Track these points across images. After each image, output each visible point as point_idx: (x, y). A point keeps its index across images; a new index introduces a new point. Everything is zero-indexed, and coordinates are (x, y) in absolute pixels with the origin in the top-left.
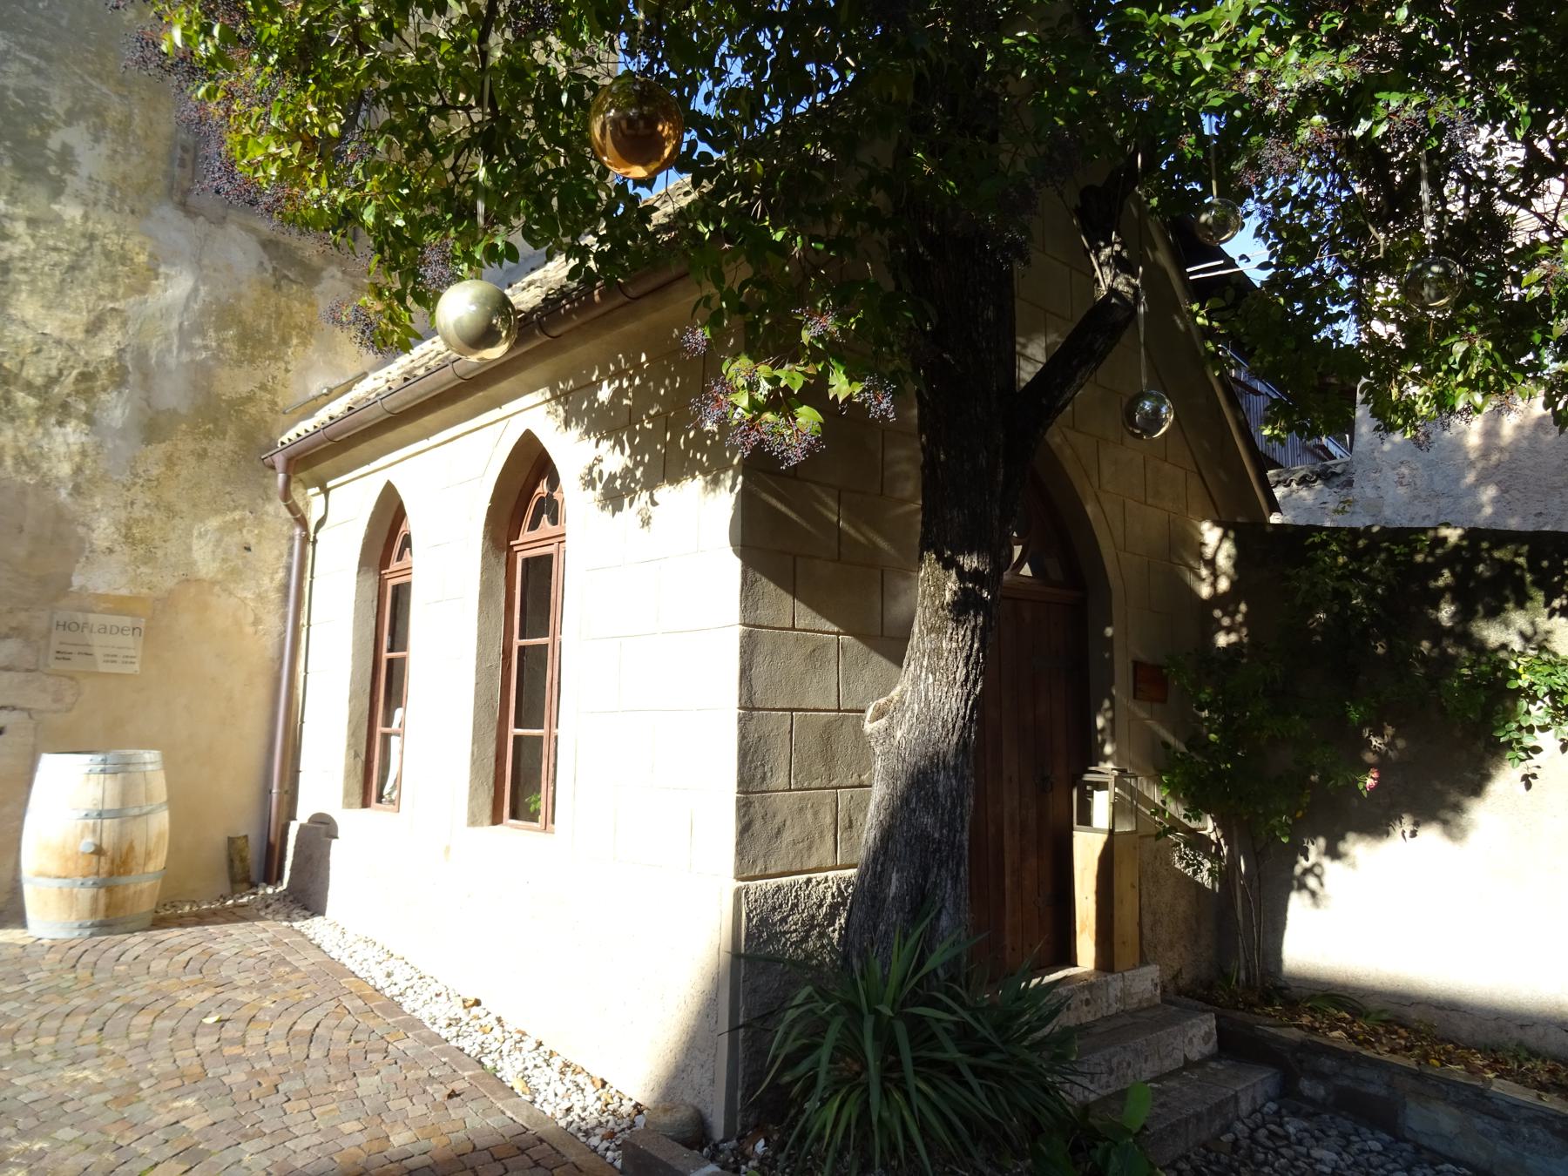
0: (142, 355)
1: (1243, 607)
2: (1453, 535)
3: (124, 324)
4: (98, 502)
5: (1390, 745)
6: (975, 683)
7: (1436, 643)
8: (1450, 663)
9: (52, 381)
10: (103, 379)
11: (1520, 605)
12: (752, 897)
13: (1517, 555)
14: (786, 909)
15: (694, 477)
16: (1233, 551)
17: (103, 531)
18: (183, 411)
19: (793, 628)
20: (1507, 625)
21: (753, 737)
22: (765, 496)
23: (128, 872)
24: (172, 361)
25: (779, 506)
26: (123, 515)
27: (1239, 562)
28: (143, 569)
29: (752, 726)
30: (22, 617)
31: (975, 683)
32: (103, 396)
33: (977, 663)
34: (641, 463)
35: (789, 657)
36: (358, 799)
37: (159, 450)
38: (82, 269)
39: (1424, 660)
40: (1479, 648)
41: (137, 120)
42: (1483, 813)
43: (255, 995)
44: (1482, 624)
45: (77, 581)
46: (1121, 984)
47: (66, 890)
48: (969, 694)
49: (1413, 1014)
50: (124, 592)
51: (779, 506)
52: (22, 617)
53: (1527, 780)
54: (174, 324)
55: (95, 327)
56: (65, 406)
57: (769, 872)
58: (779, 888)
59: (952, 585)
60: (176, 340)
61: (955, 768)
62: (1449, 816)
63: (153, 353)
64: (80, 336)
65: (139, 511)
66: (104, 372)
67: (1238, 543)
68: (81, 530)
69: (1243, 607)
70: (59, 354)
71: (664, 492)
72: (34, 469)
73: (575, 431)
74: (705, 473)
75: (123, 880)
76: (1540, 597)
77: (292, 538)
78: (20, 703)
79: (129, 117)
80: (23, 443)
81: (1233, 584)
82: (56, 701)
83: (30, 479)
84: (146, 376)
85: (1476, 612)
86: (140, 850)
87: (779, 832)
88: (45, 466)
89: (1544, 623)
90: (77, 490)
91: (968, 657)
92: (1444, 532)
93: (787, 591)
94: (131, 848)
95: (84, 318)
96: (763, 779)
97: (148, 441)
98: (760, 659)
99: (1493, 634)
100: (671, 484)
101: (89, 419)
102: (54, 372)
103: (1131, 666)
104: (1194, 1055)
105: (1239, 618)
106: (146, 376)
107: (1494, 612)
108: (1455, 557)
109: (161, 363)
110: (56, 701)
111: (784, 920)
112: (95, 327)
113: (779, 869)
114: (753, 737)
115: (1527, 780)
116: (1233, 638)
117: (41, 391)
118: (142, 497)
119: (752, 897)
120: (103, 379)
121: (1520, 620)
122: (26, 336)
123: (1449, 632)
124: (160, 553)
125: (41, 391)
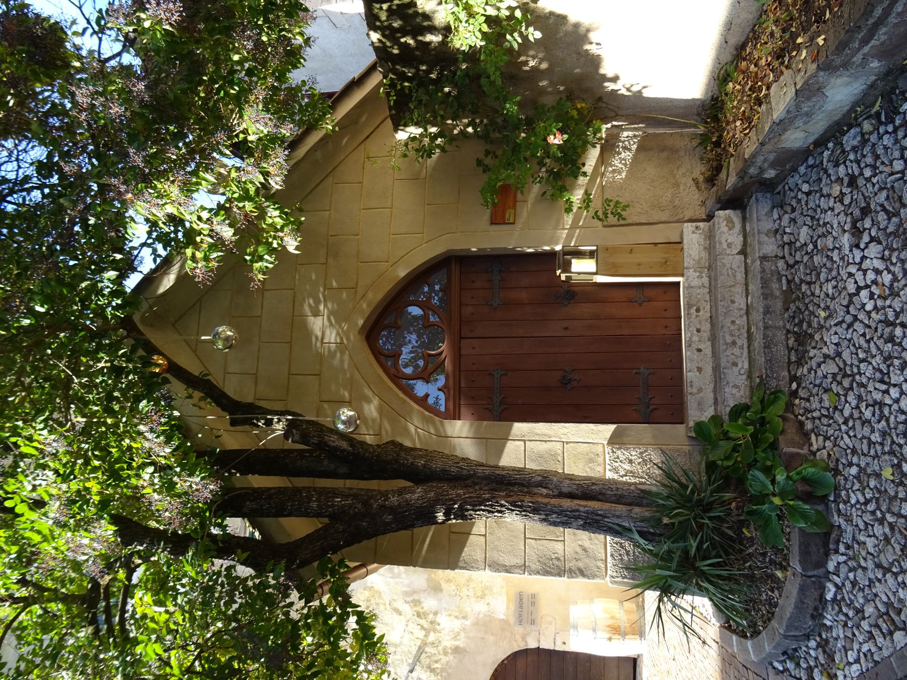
0: (406, 594)
3: (394, 600)
4: (469, 610)
5: (534, 58)
6: (502, 506)
9: (422, 627)
10: (418, 609)
12: (615, 574)
13: (381, 8)
14: (623, 552)
17: (480, 607)
18: (426, 576)
19: (485, 535)
21: (538, 566)
22: (424, 552)
23: (619, 627)
24: (406, 582)
25: (427, 542)
26: (473, 599)
28: (495, 590)
29: (533, 567)
30: (518, 637)
31: (502, 506)
32: (425, 608)
33: (491, 506)
35: (499, 539)
37: (444, 585)
43: (753, 134)
45: (502, 617)
46: (691, 270)
48: (508, 509)
49: (734, 40)
50: (505, 598)
51: (427, 542)
52: (518, 637)
54: (391, 580)
55: (399, 613)
56: (432, 623)
57: (604, 558)
58: (612, 555)
60: (398, 580)
61: (546, 515)
63: (404, 589)
64: (402, 617)
65: (471, 594)
68: (481, 616)
70: (410, 624)
72: (458, 634)
75: (622, 629)
78: (553, 637)
80: (449, 638)
82: (551, 624)
83: (462, 635)
84: (414, 592)
85: (429, 26)
86: (610, 622)
87: (585, 550)
88: (457, 630)
90: (464, 618)
91: (489, 512)
93: (467, 539)
94: (609, 626)
95: (395, 616)
96: (558, 559)
97: (441, 590)
98: (501, 559)
101: (436, 613)
103: (495, 227)
104: (738, 241)
106: (414, 592)
108: (389, 33)
110: (551, 624)
111: (628, 553)
112: (399, 613)
113: (603, 551)
114: (538, 566)
117: (427, 632)
118: (465, 592)
119: (615, 574)
120: (418, 609)
124: (487, 584)
125: (427, 632)
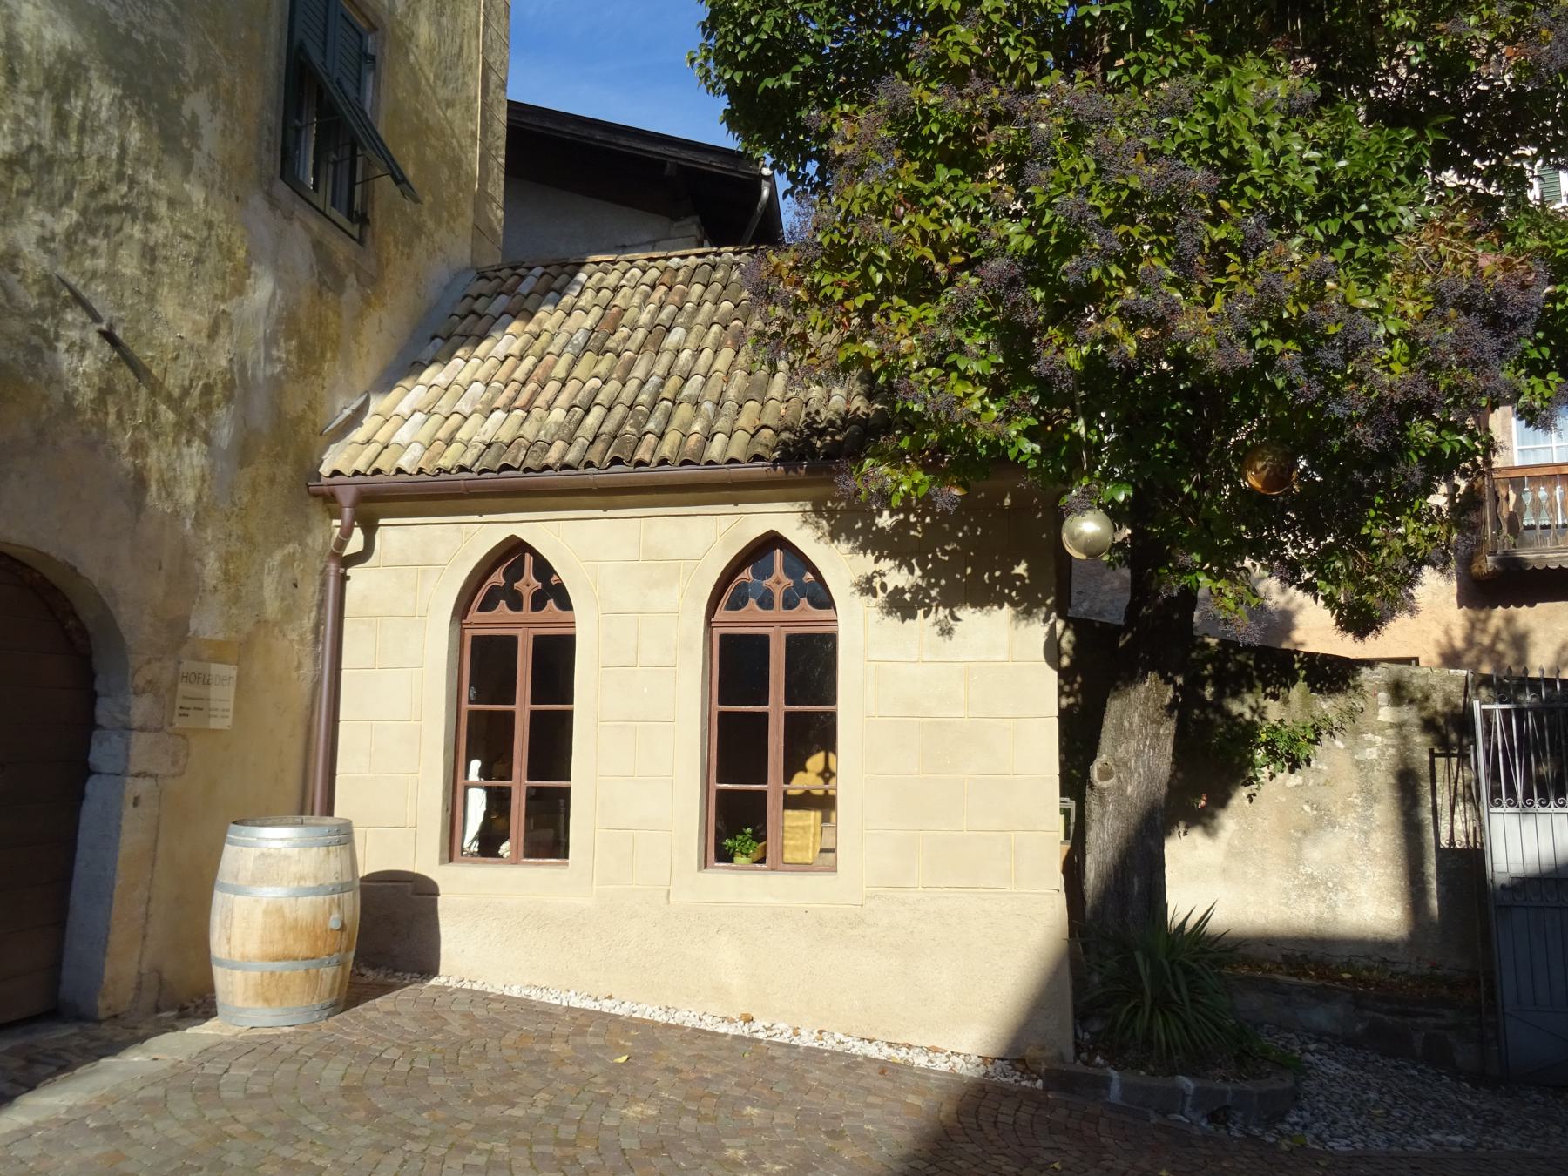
1: (1079, 679)
2: (1213, 642)
7: (1202, 712)
8: (1209, 723)
11: (1250, 690)
15: (1001, 607)
16: (1073, 638)
20: (1243, 701)
27: (1077, 647)
34: (937, 584)
36: (447, 855)
38: (203, 262)
39: (1196, 722)
40: (1227, 715)
41: (239, 89)
42: (1230, 821)
44: (1229, 700)
47: (312, 971)
50: (220, 637)
53: (1251, 797)
59: (1170, 694)
62: (1207, 821)
66: (220, 385)
67: (1076, 633)
69: (1079, 679)
71: (966, 614)
73: (844, 547)
74: (1013, 604)
76: (1260, 685)
77: (324, 572)
79: (233, 85)
81: (1072, 661)
89: (1263, 703)
92: (1208, 640)
99: (1235, 707)
100: (973, 606)
102: (187, 383)
105: (1076, 686)
107: (1236, 694)
109: (254, 376)
115: (1251, 797)
116: (1072, 700)
121: (1250, 699)
122: (169, 339)
123: (1210, 704)
